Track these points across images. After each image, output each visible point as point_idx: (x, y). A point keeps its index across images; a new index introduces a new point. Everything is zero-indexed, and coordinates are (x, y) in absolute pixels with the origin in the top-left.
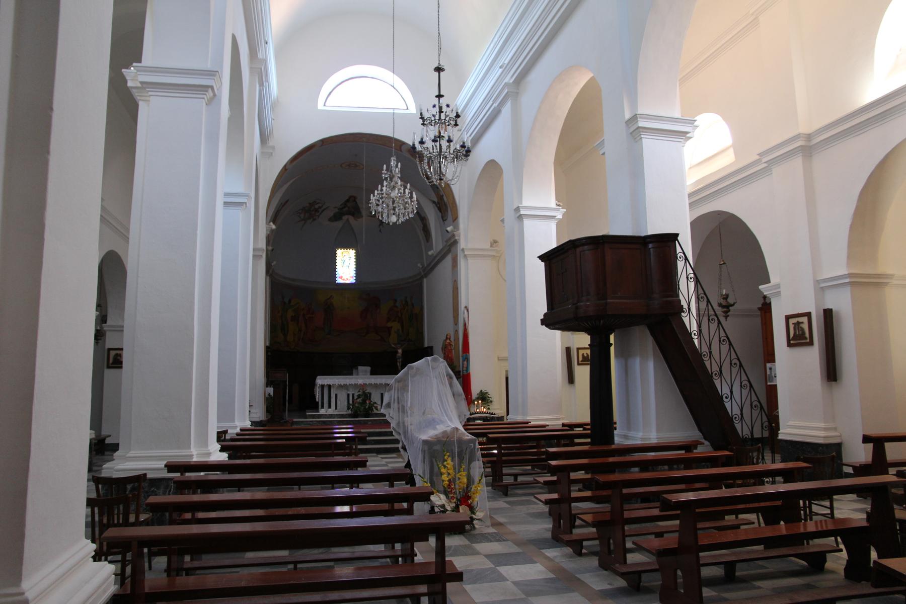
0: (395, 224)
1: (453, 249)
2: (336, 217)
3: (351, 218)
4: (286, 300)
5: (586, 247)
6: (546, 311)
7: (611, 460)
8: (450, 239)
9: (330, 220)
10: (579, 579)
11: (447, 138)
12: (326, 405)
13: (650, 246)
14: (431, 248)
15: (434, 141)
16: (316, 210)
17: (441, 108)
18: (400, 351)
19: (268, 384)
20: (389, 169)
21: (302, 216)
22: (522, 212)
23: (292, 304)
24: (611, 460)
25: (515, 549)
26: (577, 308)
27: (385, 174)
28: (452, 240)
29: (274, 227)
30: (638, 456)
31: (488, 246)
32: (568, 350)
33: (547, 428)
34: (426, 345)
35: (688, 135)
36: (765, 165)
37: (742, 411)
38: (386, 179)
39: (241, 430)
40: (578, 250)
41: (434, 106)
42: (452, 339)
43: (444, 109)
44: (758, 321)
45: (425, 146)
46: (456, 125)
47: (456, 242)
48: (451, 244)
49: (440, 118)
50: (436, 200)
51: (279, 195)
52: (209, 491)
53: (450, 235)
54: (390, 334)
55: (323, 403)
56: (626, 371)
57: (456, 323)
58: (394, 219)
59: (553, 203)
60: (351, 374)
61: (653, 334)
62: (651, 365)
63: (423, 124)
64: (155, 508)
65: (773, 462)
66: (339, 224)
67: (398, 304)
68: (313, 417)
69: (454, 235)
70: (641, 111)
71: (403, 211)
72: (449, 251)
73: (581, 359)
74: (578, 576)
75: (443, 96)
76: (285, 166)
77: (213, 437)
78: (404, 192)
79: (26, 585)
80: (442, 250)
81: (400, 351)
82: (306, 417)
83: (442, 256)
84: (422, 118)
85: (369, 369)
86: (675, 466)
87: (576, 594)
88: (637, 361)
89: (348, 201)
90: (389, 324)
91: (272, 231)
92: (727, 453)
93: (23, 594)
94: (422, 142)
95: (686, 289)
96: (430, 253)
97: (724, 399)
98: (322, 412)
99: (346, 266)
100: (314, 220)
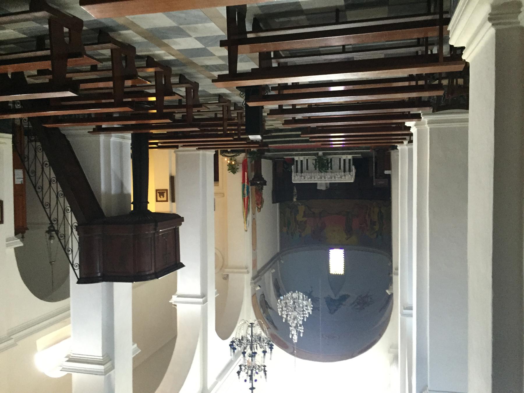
0: (294, 292)
1: (256, 273)
2: (344, 298)
3: (333, 297)
5: (147, 273)
6: (181, 228)
7: (133, 122)
8: (258, 281)
9: (348, 296)
10: (145, 38)
11: (246, 355)
12: (347, 162)
13: (99, 275)
14: (273, 274)
15: (255, 353)
16: (359, 303)
17: (251, 379)
18: (295, 200)
19: (389, 177)
20: (299, 333)
22: (201, 300)
24: (133, 122)
25: (196, 60)
26: (155, 229)
27: (301, 329)
28: (256, 280)
29: (387, 291)
30: (116, 125)
31: (230, 275)
32: (173, 200)
34: (278, 204)
35: (67, 359)
36: (12, 337)
37: (36, 154)
38: (300, 326)
39: (402, 143)
40: (153, 271)
41: (256, 381)
42: (257, 208)
43: (248, 379)
44: (30, 219)
45: (262, 349)
46: (240, 366)
47: (254, 278)
48: (257, 277)
49: (252, 371)
50: (269, 310)
51: (386, 315)
53: (258, 284)
54: (304, 212)
55: (350, 163)
56: (122, 185)
57: (254, 220)
58: (295, 295)
62: (103, 188)
63: (265, 366)
64: (439, 87)
65: (21, 119)
66: (342, 293)
68: (356, 153)
69: (255, 283)
70: (102, 378)
71: (287, 301)
72: (259, 272)
73: (165, 194)
74: (145, 40)
75: (254, 388)
77: (415, 138)
78: (287, 315)
79: (493, 31)
80: (265, 273)
81: (295, 200)
82: (361, 153)
83: (265, 268)
84: (265, 371)
85: (318, 188)
87: (145, 28)
88: (113, 192)
89: (335, 310)
90: (305, 219)
91: (388, 289)
92: (47, 126)
93: (493, 25)
94: (265, 352)
95: (74, 244)
96: (274, 271)
97: (48, 163)
98: (350, 157)
99: (337, 261)
100: (360, 296)
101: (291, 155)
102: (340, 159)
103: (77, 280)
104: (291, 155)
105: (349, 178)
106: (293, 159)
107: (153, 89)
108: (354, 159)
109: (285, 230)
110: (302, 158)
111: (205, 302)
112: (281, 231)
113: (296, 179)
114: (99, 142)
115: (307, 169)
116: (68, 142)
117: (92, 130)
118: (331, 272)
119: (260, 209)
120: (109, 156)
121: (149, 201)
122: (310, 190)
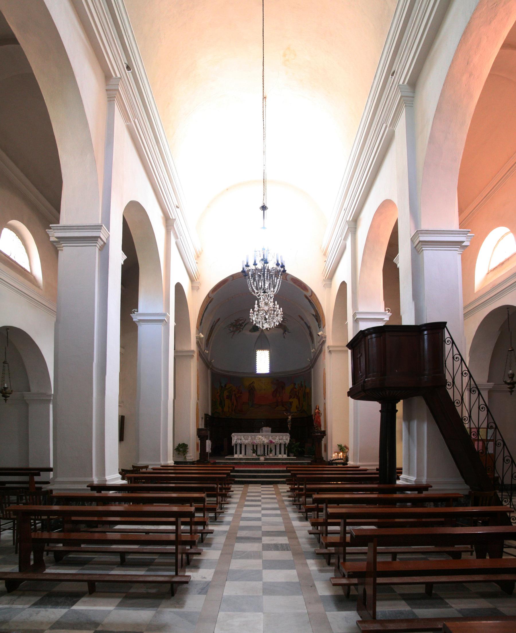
4: (223, 385)
9: (250, 331)
12: (238, 452)
16: (241, 325)
18: (290, 417)
21: (231, 329)
23: (227, 387)
33: (368, 472)
45: (257, 266)
47: (324, 342)
50: (314, 314)
52: (104, 504)
58: (266, 326)
59: (382, 309)
60: (259, 432)
61: (427, 403)
67: (296, 386)
68: (229, 459)
76: (208, 294)
81: (290, 417)
86: (439, 503)
90: (291, 400)
98: (236, 456)
99: (263, 362)
100: (240, 331)
101: (290, 459)
102: (245, 454)
103: (447, 325)
104: (290, 459)
105: (237, 438)
106: (288, 456)
107: (330, 530)
108: (232, 454)
109: (307, 391)
110: (280, 456)
111: (354, 315)
112: (311, 388)
113: (284, 438)
114: (428, 476)
115: (276, 446)
116: (463, 477)
117: (429, 488)
118: (268, 352)
119: (316, 408)
120: (417, 461)
121: (380, 413)
122: (278, 427)
